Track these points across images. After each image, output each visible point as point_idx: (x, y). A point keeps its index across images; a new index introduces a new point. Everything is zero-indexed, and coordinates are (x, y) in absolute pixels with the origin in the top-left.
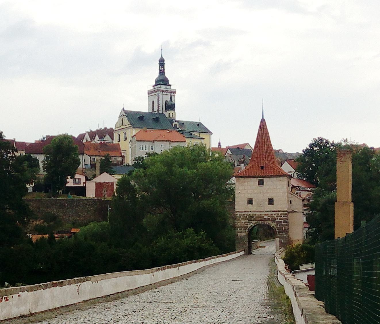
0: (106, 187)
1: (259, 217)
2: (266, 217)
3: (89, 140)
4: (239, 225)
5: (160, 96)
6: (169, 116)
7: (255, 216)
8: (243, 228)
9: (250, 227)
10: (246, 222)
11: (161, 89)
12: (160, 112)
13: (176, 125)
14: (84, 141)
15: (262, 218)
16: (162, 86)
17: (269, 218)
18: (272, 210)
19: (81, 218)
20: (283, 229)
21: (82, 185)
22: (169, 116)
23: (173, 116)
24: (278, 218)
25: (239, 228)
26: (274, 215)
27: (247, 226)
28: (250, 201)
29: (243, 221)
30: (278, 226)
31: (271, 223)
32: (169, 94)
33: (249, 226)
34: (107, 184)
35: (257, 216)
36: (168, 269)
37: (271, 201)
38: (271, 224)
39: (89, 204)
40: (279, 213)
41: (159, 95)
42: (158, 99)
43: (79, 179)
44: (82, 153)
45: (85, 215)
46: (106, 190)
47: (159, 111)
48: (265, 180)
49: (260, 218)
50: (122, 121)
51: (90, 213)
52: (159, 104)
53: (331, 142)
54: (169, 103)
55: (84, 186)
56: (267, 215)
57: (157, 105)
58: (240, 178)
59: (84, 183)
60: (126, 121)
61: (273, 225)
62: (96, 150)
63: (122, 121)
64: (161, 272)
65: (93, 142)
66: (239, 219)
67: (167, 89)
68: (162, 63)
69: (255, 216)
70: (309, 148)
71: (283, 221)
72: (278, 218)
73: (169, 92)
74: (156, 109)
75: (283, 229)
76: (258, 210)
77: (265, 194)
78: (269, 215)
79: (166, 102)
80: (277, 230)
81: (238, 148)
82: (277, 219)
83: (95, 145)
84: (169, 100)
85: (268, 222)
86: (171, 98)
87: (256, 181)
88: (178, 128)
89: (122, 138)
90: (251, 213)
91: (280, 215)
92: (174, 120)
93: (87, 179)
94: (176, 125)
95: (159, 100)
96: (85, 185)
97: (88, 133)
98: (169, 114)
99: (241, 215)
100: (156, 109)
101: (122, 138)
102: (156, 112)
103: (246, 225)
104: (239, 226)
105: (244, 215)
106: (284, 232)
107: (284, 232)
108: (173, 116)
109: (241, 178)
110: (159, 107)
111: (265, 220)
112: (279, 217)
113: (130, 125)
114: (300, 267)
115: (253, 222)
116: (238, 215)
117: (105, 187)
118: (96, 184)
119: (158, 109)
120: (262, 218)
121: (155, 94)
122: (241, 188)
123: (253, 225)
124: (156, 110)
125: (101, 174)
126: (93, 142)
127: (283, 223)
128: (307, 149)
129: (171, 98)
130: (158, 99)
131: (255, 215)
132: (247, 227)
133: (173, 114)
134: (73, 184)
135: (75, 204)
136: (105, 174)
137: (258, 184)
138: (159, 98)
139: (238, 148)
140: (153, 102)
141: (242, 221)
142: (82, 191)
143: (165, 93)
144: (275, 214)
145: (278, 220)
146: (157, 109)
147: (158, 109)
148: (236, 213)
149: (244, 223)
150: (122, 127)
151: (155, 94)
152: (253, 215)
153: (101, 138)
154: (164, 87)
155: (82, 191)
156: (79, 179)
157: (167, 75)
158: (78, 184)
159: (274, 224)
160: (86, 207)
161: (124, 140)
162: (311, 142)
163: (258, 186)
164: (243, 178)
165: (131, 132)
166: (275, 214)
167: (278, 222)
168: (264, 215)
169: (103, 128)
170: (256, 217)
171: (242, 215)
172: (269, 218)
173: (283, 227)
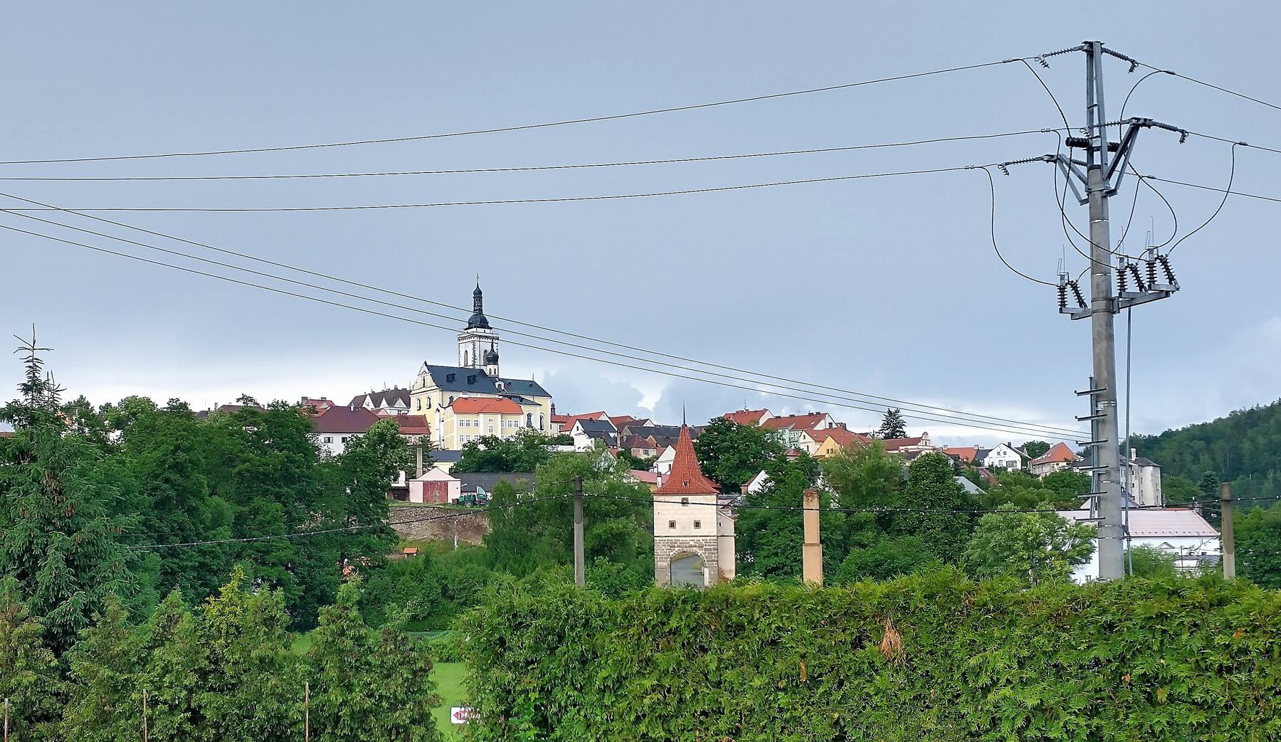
2: (692, 543)
5: (477, 343)
6: (490, 373)
12: (477, 367)
13: (500, 385)
16: (479, 330)
23: (495, 373)
31: (698, 551)
33: (671, 553)
37: (697, 524)
50: (424, 380)
52: (475, 356)
56: (694, 540)
60: (429, 379)
61: (700, 552)
63: (424, 380)
68: (478, 294)
74: (470, 363)
76: (682, 535)
81: (591, 419)
85: (695, 549)
86: (492, 347)
89: (424, 403)
90: (673, 538)
94: (500, 385)
100: (470, 363)
101: (424, 403)
102: (471, 367)
106: (714, 561)
107: (714, 561)
108: (495, 373)
111: (691, 546)
113: (436, 387)
115: (677, 549)
119: (474, 362)
121: (469, 340)
129: (492, 347)
139: (591, 419)
145: (707, 547)
148: (655, 538)
150: (424, 389)
151: (469, 340)
152: (675, 540)
154: (482, 330)
165: (436, 397)
167: (705, 549)
169: (392, 388)
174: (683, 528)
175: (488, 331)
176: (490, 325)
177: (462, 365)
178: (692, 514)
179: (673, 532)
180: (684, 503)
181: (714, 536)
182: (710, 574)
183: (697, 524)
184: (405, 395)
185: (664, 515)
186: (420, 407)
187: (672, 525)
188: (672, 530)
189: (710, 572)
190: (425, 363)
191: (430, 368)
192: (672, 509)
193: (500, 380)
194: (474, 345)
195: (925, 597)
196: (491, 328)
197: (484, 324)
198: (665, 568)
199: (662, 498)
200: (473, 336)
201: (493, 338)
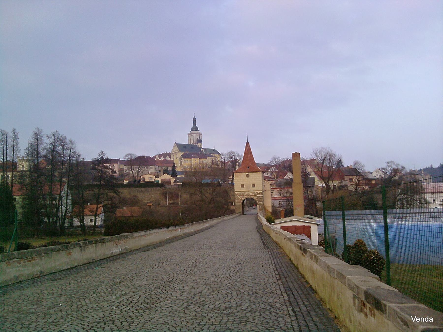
2: (251, 194)
6: (199, 146)
13: (202, 150)
28: (243, 186)
40: (258, 192)
48: (250, 174)
56: (252, 193)
59: (154, 180)
61: (255, 198)
68: (194, 120)
74: (192, 143)
86: (200, 137)
94: (202, 150)
106: (261, 202)
107: (261, 202)
111: (251, 195)
115: (245, 197)
129: (200, 137)
144: (256, 193)
152: (244, 193)
167: (258, 197)
176: (199, 130)
179: (243, 189)
180: (248, 176)
181: (261, 191)
182: (260, 208)
184: (169, 155)
186: (177, 158)
188: (243, 188)
190: (175, 143)
192: (242, 179)
195: (239, 287)
196: (199, 131)
197: (196, 129)
199: (351, 212)
200: (193, 133)
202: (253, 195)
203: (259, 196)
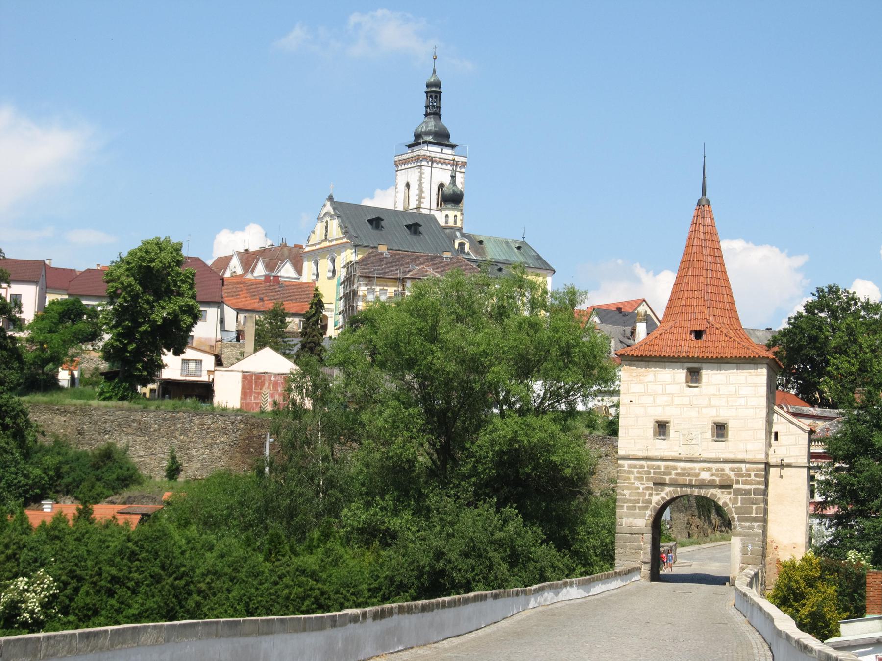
0: (269, 387)
1: (684, 475)
2: (705, 476)
3: (239, 271)
4: (627, 495)
6: (447, 222)
7: (674, 472)
8: (637, 505)
9: (659, 501)
10: (648, 488)
11: (428, 154)
12: (425, 212)
14: (227, 275)
15: (694, 479)
16: (432, 148)
17: (714, 478)
18: (723, 456)
19: (195, 465)
20: (754, 511)
21: (204, 378)
22: (447, 222)
23: (455, 222)
24: (740, 479)
25: (625, 505)
26: (727, 472)
27: (651, 501)
28: (662, 428)
29: (640, 485)
30: (739, 504)
32: (449, 167)
34: (273, 379)
35: (679, 471)
36: (400, 616)
37: (720, 430)
38: (718, 496)
39: (218, 428)
41: (423, 167)
42: (421, 178)
43: (199, 362)
44: (217, 299)
45: (205, 456)
46: (269, 394)
47: (421, 210)
49: (688, 478)
50: (326, 228)
51: (219, 451)
53: (863, 300)
54: (448, 190)
55: (211, 380)
56: (709, 469)
57: (417, 192)
58: (634, 361)
59: (210, 372)
62: (253, 296)
63: (326, 228)
64: (603, 586)
65: (249, 276)
66: (629, 479)
67: (442, 156)
68: (434, 92)
69: (674, 472)
70: (804, 314)
71: (754, 489)
72: (740, 479)
73: (449, 163)
75: (754, 511)
76: (683, 455)
77: (704, 411)
78: (714, 472)
79: (441, 186)
80: (736, 514)
81: (619, 310)
82: (738, 482)
83: (253, 284)
84: (447, 181)
87: (680, 374)
88: (468, 254)
91: (744, 472)
92: (458, 234)
93: (219, 362)
94: (462, 245)
95: (423, 180)
96: (213, 379)
97: (239, 253)
98: (447, 216)
99: (635, 467)
102: (415, 211)
103: (647, 497)
104: (627, 497)
105: (642, 467)
106: (755, 520)
109: (638, 361)
110: (420, 197)
111: (702, 485)
112: (743, 477)
114: (843, 628)
116: (626, 465)
117: (267, 384)
118: (244, 377)
120: (694, 479)
122: (637, 388)
123: (668, 499)
124: (415, 206)
125: (256, 350)
126: (249, 276)
127: (753, 496)
128: (799, 316)
129: (453, 177)
130: (421, 178)
131: (675, 468)
132: (650, 502)
133: (456, 216)
134: (182, 375)
135: (179, 426)
136: (267, 352)
137: (687, 382)
138: (423, 176)
140: (408, 185)
141: (637, 484)
142: (205, 391)
143: (439, 166)
144: (732, 470)
145: (740, 486)
146: (418, 202)
147: (420, 202)
149: (641, 490)
152: (667, 467)
153: (270, 267)
154: (437, 149)
155: (205, 391)
156: (199, 362)
157: (447, 120)
158: (195, 375)
159: (728, 496)
160: (208, 434)
161: (329, 278)
162: (810, 299)
163: (684, 385)
164: (642, 361)
166: (732, 470)
167: (737, 492)
168: (699, 469)
170: (677, 474)
171: (637, 468)
172: (714, 478)
173: (754, 507)
174: (688, 441)
175: (447, 151)
177: (400, 208)
178: (709, 406)
183: (720, 430)
185: (643, 406)
187: (662, 428)
189: (744, 545)
191: (336, 205)
193: (464, 235)
194: (421, 173)
198: (680, 558)
200: (418, 159)
201: (455, 164)
202: (715, 486)
203: (748, 492)
